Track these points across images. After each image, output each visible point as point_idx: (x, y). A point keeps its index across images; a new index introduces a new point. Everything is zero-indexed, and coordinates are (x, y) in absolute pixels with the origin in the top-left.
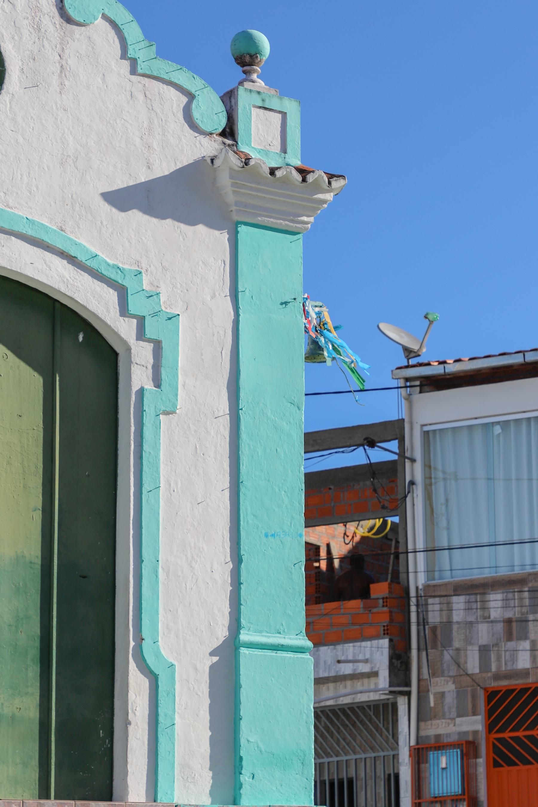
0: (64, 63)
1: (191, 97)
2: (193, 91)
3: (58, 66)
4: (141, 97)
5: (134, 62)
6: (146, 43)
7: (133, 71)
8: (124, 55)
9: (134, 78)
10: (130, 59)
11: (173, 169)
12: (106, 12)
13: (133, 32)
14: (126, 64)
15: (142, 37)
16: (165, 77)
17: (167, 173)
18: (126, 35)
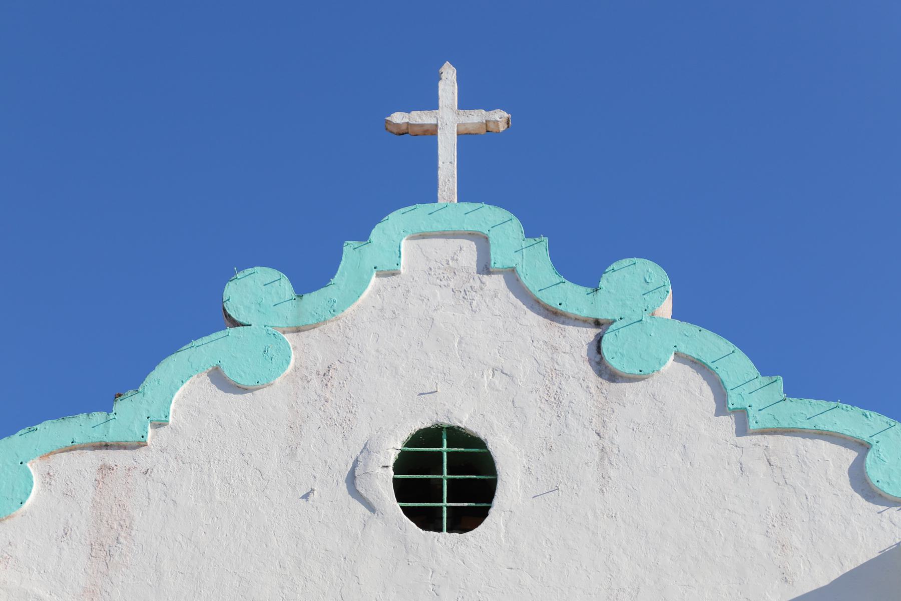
0: (606, 443)
1: (863, 447)
2: (865, 437)
3: (596, 451)
4: (761, 468)
5: (741, 418)
6: (766, 380)
7: (742, 429)
8: (722, 408)
9: (744, 440)
10: (734, 411)
11: (836, 573)
12: (683, 349)
13: (736, 366)
14: (728, 423)
15: (754, 372)
16: (807, 425)
17: (824, 583)
18: (723, 375)
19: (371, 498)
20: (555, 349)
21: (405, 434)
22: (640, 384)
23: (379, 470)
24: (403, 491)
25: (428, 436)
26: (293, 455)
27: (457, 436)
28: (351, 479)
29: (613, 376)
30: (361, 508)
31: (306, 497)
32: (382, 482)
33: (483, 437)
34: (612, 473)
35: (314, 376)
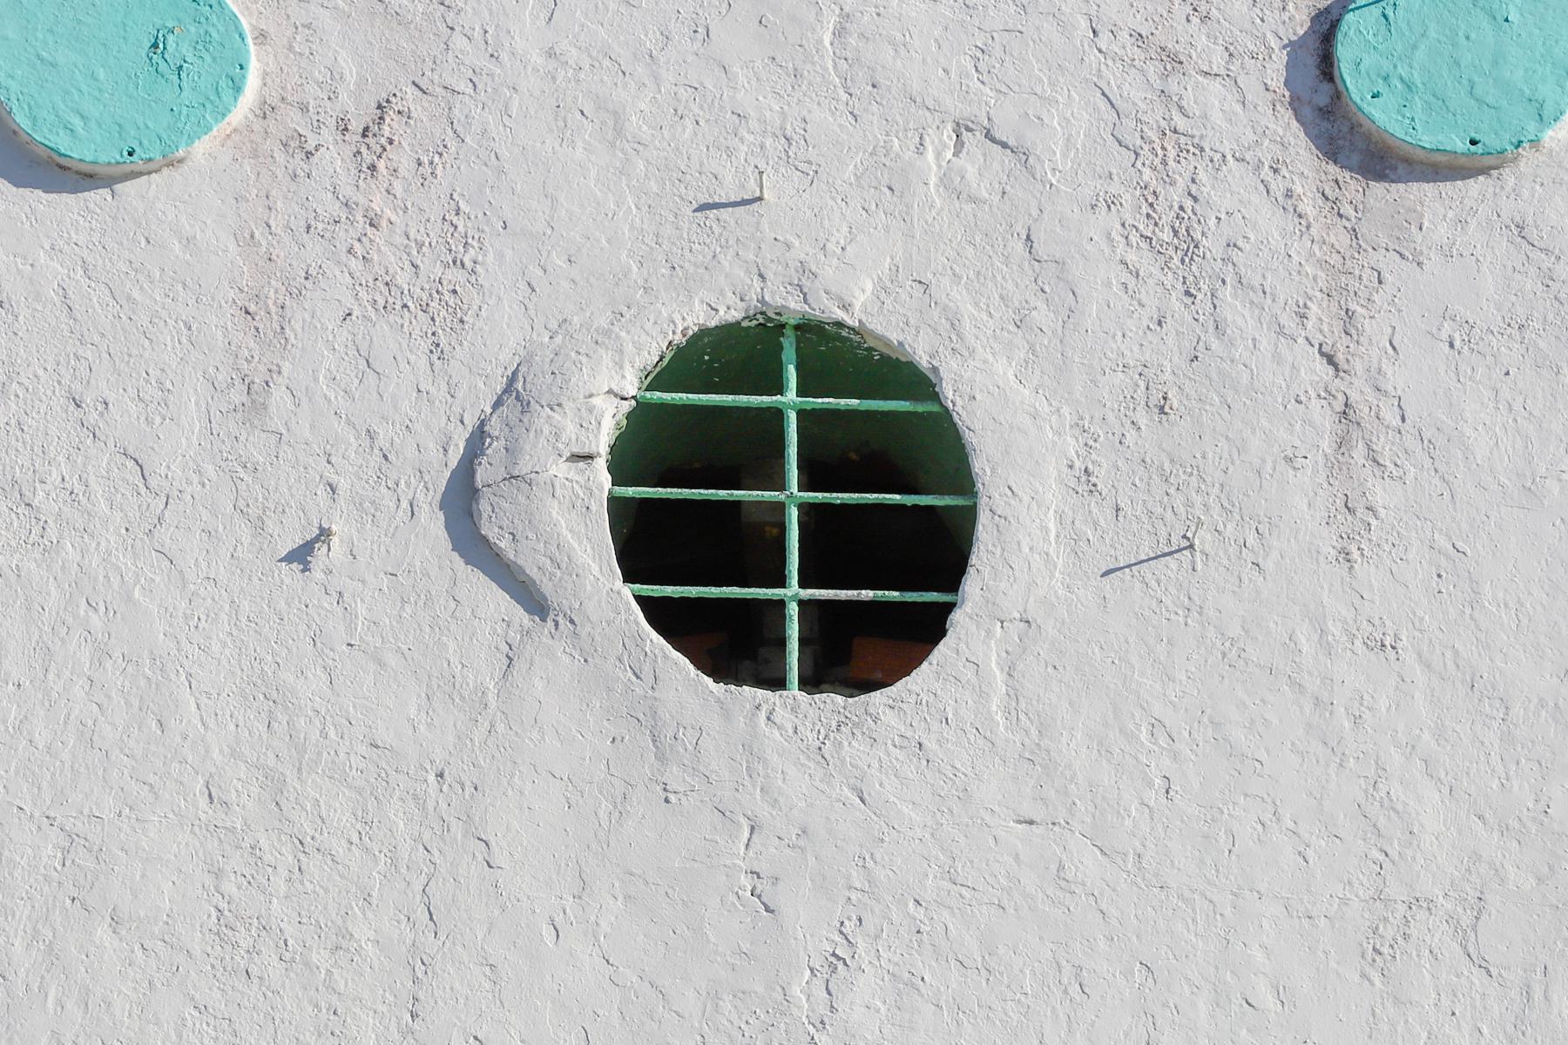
0: (1360, 391)
19: (531, 562)
20: (1173, 60)
21: (650, 346)
22: (1475, 186)
23: (561, 470)
24: (645, 543)
25: (735, 354)
26: (254, 407)
27: (834, 354)
28: (462, 499)
29: (1378, 159)
30: (496, 601)
31: (301, 556)
32: (570, 516)
33: (923, 362)
34: (1381, 493)
35: (328, 135)
